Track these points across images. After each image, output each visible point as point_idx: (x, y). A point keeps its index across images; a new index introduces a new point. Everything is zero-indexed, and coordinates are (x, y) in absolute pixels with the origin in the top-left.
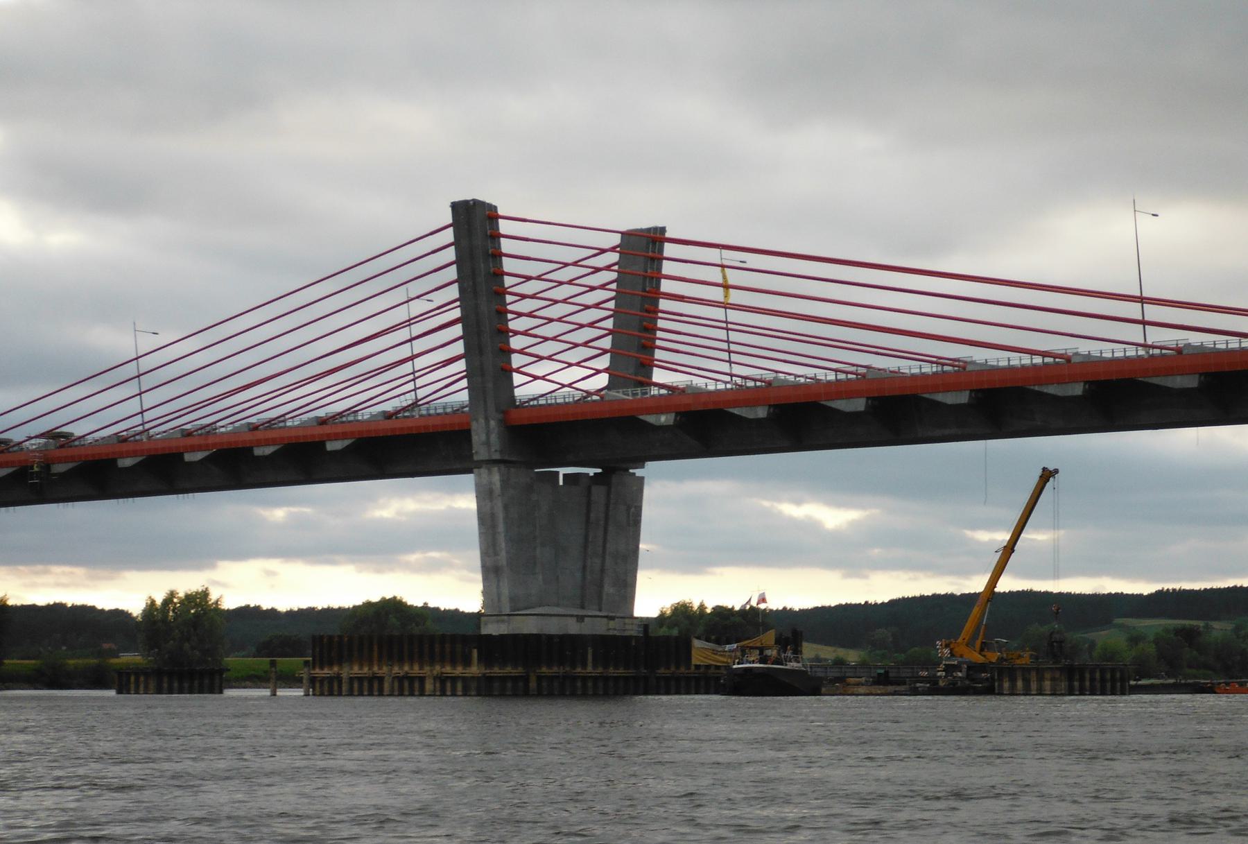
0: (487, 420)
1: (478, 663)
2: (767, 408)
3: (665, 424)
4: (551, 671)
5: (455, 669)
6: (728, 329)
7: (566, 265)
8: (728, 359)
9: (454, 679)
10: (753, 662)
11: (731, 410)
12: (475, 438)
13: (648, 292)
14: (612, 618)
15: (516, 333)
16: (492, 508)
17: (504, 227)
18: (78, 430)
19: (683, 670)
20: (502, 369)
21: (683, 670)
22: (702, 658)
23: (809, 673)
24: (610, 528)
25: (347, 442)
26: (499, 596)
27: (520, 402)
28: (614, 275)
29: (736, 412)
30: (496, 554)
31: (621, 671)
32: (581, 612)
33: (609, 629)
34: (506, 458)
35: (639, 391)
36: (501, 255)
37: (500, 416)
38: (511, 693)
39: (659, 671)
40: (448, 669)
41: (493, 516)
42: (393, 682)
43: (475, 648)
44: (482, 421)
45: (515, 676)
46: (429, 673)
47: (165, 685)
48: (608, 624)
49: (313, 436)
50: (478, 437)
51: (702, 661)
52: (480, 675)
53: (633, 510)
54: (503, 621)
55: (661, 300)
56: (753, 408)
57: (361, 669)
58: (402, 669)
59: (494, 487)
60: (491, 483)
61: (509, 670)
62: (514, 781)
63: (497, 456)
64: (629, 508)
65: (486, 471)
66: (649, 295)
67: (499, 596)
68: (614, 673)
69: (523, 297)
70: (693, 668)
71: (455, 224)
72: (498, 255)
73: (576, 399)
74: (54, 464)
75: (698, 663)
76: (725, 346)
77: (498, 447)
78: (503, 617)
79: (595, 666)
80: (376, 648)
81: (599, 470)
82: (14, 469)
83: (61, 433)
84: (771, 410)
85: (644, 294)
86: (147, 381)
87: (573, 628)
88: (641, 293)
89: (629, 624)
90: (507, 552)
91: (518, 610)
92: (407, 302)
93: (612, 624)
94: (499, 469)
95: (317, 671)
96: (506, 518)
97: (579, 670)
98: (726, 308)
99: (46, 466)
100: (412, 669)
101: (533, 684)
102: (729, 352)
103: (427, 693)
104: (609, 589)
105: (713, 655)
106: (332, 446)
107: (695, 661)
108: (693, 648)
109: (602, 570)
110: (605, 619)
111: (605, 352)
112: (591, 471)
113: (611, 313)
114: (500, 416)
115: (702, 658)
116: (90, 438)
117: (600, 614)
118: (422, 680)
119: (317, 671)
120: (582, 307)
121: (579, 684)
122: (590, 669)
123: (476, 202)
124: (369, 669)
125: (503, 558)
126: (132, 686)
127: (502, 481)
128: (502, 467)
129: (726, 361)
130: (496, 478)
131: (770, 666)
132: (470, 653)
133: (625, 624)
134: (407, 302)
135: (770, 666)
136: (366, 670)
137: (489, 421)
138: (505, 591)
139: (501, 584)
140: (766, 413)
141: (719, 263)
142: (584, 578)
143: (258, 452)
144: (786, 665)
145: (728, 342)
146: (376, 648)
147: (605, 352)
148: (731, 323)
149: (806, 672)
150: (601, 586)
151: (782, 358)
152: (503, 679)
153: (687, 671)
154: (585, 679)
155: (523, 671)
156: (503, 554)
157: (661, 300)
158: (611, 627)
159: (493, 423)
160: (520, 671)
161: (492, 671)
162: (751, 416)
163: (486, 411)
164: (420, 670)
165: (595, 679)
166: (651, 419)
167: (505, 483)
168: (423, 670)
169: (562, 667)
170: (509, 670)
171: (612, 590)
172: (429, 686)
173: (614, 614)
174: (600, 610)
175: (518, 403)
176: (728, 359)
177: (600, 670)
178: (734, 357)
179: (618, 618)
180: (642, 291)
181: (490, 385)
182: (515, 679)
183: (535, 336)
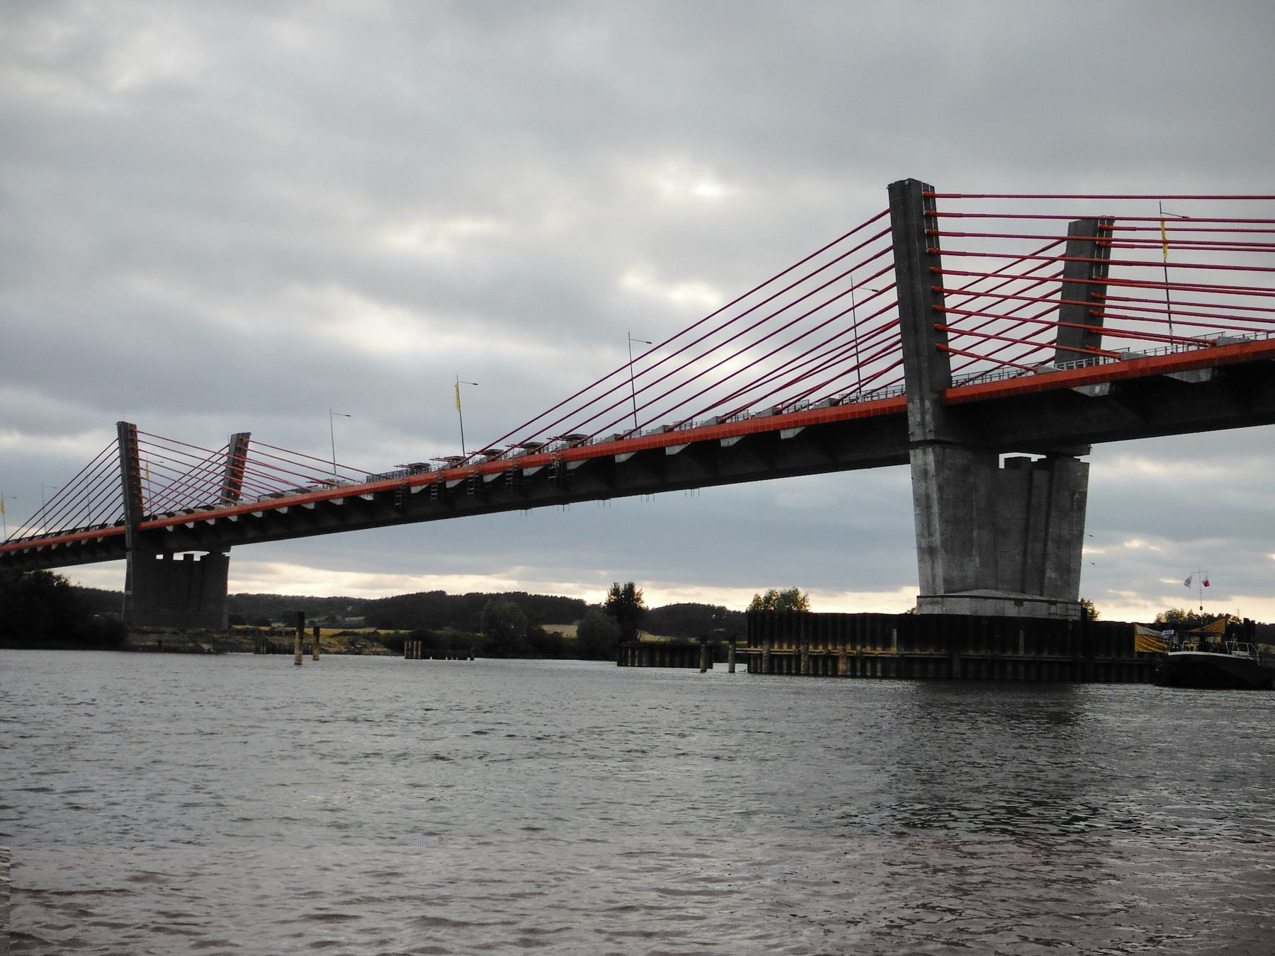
0: (922, 400)
1: (897, 643)
2: (1210, 370)
3: (1100, 395)
4: (976, 654)
5: (874, 650)
6: (1168, 303)
7: (1023, 258)
8: (1168, 319)
9: (874, 660)
10: (1192, 649)
11: (1171, 375)
12: (911, 420)
13: (1094, 280)
14: (1054, 603)
15: (951, 292)
16: (927, 488)
17: (941, 205)
18: (584, 431)
19: (1124, 657)
20: (938, 349)
21: (1124, 657)
22: (1146, 646)
23: (1259, 664)
24: (1053, 513)
25: (798, 430)
26: (934, 577)
27: (957, 383)
28: (1060, 285)
29: (1176, 377)
30: (930, 535)
31: (1056, 656)
32: (1020, 596)
33: (1050, 614)
34: (941, 438)
35: (1074, 365)
36: (938, 234)
37: (936, 396)
38: (894, 675)
39: (1098, 658)
40: (868, 649)
41: (928, 497)
42: (809, 661)
43: (895, 628)
44: (917, 401)
45: (1028, 661)
46: (842, 653)
47: (658, 659)
48: (1050, 607)
49: (769, 426)
50: (914, 418)
51: (1147, 649)
52: (898, 656)
53: (1077, 496)
54: (937, 603)
55: (1108, 287)
56: (1195, 371)
57: (789, 647)
58: (855, 649)
59: (929, 468)
60: (926, 464)
61: (930, 652)
62: (344, 936)
63: (931, 437)
64: (1073, 493)
65: (922, 451)
66: (1094, 282)
67: (934, 577)
68: (1047, 658)
69: (962, 333)
70: (1136, 655)
71: (893, 210)
72: (935, 235)
73: (1011, 376)
74: (569, 461)
75: (1142, 650)
76: (1164, 307)
77: (932, 427)
78: (936, 599)
79: (1027, 650)
80: (802, 626)
81: (1044, 457)
82: (540, 468)
83: (574, 435)
84: (1216, 372)
85: (1089, 281)
86: (639, 383)
87: (1011, 610)
88: (1087, 281)
89: (1072, 610)
90: (942, 534)
91: (955, 592)
92: (851, 290)
93: (1053, 609)
94: (933, 449)
95: (752, 648)
96: (941, 499)
97: (1009, 654)
98: (1167, 283)
99: (563, 464)
100: (836, 649)
101: (957, 667)
102: (1170, 313)
103: (839, 673)
104: (1050, 574)
105: (1157, 643)
106: (786, 434)
107: (1137, 649)
108: (1136, 636)
109: (1045, 555)
110: (1046, 604)
111: (1052, 325)
112: (1035, 458)
113: (1057, 304)
114: (936, 396)
115: (1146, 646)
116: (597, 439)
117: (1041, 598)
118: (835, 659)
119: (752, 648)
120: (1047, 325)
121: (1009, 668)
122: (1021, 653)
123: (912, 182)
124: (797, 648)
125: (937, 539)
126: (630, 661)
127: (937, 462)
128: (938, 448)
129: (1167, 322)
130: (931, 458)
131: (1212, 654)
132: (890, 634)
133: (1067, 609)
134: (851, 290)
135: (1212, 654)
136: (821, 648)
137: (924, 402)
138: (940, 572)
139: (936, 565)
140: (1210, 375)
141: (1159, 216)
142: (1025, 563)
143: (724, 443)
144: (1230, 654)
145: (1168, 303)
146: (802, 626)
147: (1052, 325)
148: (1158, 229)
149: (1254, 662)
150: (1043, 572)
151: (1229, 315)
152: (924, 661)
153: (1129, 659)
154: (1015, 663)
155: (946, 653)
156: (938, 535)
157: (1108, 287)
158: (1052, 612)
159: (927, 403)
160: (942, 653)
161: (912, 652)
162: (1193, 381)
163: (921, 390)
164: (816, 649)
165: (1027, 664)
166: (1084, 390)
167: (940, 464)
168: (818, 649)
169: (989, 651)
170: (930, 652)
171: (1053, 575)
172: (842, 666)
173: (1054, 599)
174: (1041, 595)
175: (954, 385)
176: (1168, 319)
177: (1033, 654)
178: (1174, 317)
179: (1059, 603)
180: (1089, 279)
181: (925, 365)
182: (937, 661)
183: (968, 293)
